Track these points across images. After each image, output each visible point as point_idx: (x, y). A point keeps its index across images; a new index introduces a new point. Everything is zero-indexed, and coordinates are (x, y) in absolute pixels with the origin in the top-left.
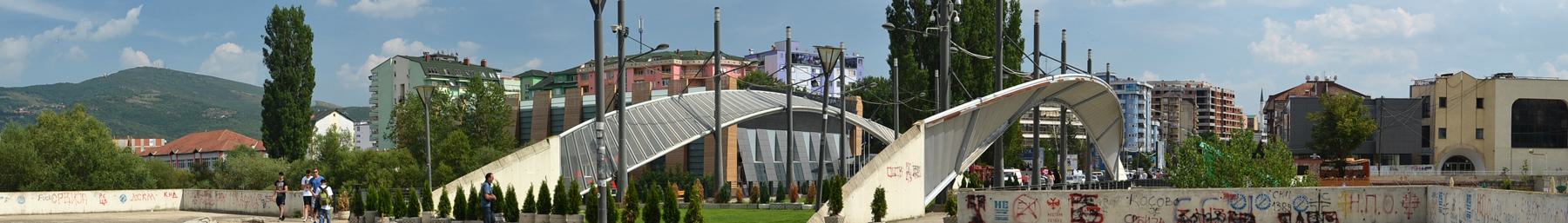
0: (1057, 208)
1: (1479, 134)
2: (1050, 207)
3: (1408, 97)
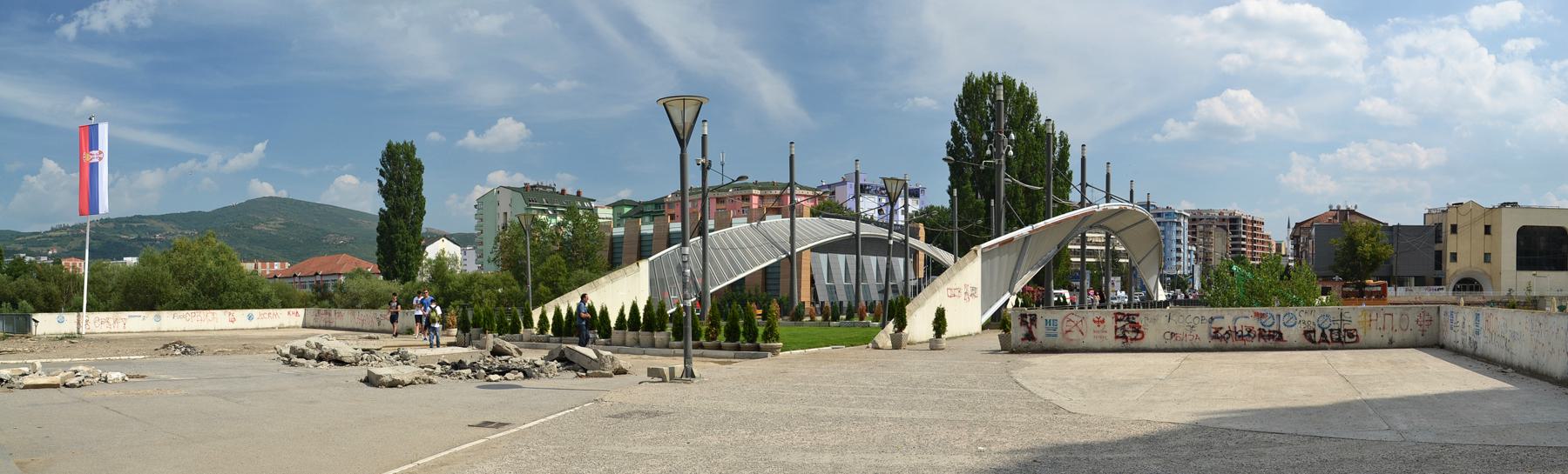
0: (1102, 325)
1: (1487, 258)
3: (1423, 224)
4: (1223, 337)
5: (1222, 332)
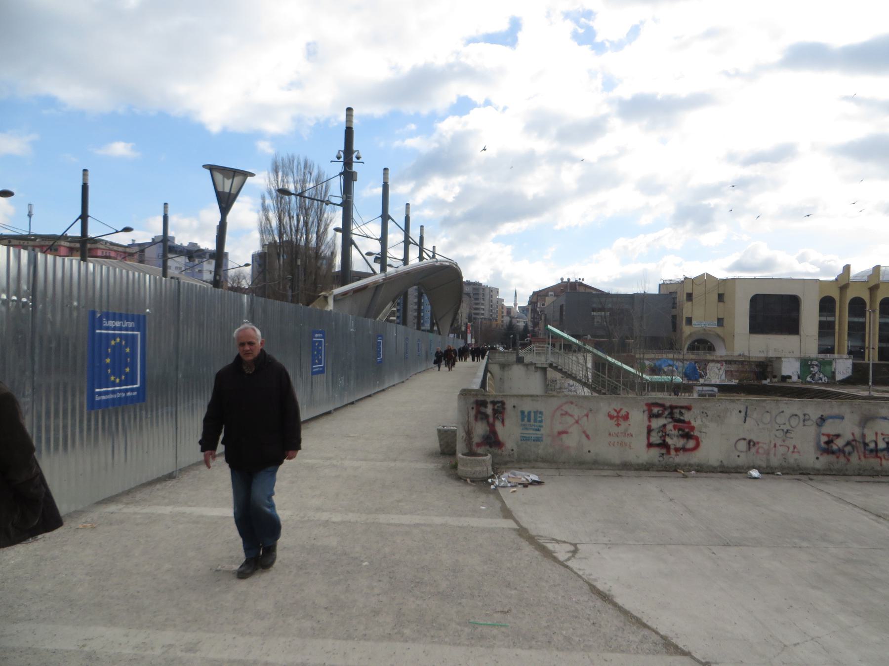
0: (624, 424)
1: (720, 322)
2: (613, 422)
3: (658, 293)
4: (841, 451)
5: (839, 443)
